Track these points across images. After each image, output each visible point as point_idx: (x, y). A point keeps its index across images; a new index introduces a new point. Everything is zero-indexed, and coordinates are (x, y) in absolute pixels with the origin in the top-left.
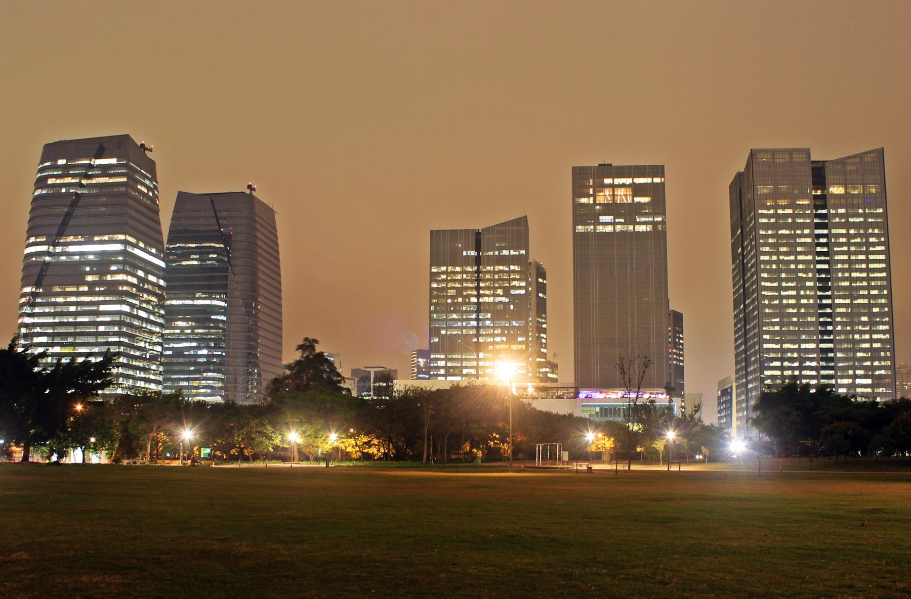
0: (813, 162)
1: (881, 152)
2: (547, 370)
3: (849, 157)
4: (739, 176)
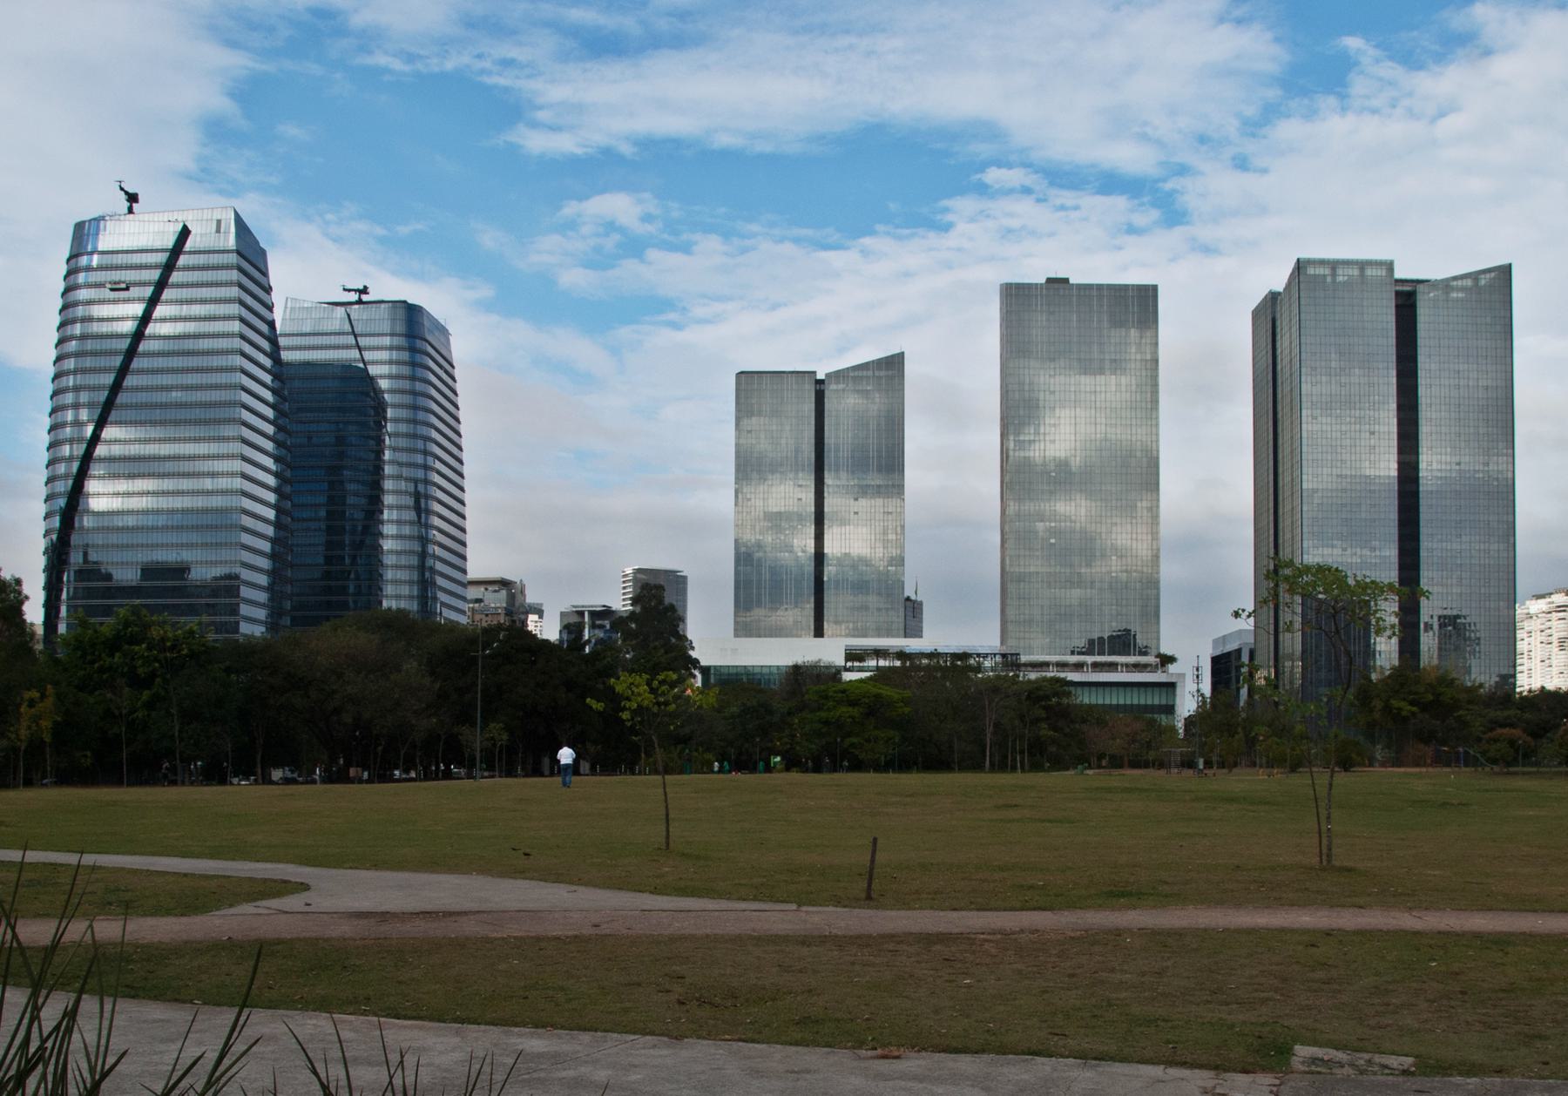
0: (1397, 281)
1: (1505, 272)
2: (848, 676)
3: (1455, 278)
4: (1273, 297)
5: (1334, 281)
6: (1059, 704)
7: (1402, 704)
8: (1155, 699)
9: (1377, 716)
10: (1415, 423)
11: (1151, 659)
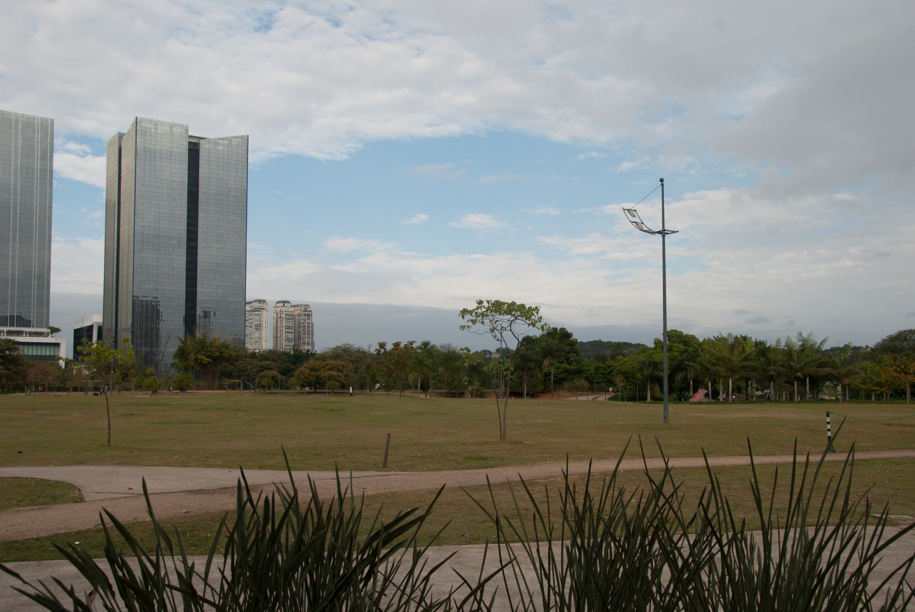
5: (156, 133)
6: (10, 355)
7: (203, 357)
8: (48, 352)
9: (192, 363)
10: (196, 210)
11: (45, 330)
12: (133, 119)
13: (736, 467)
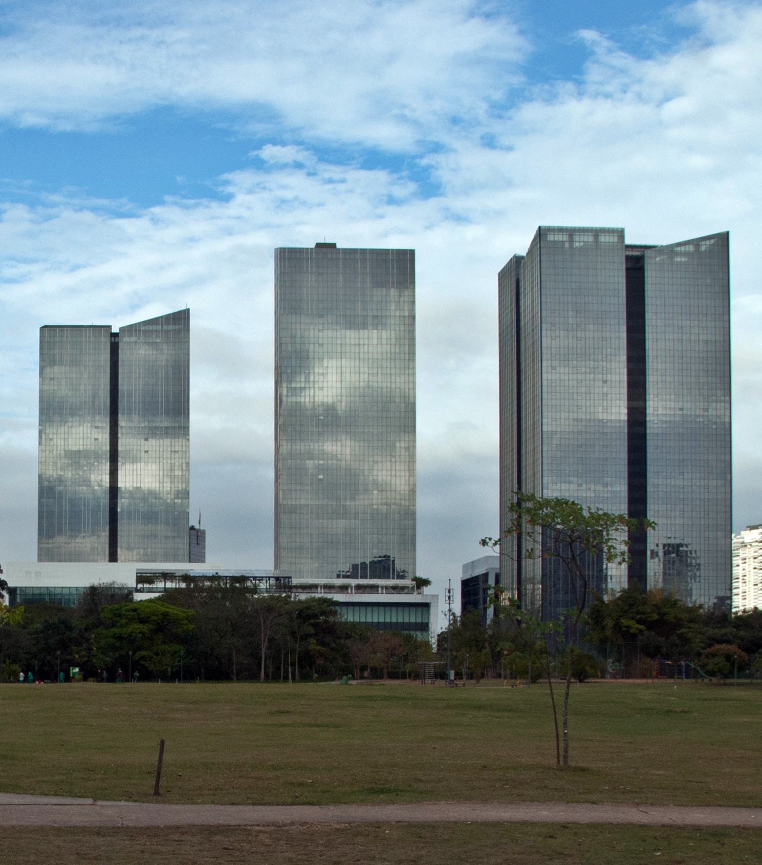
6: (326, 622)
7: (631, 623)
8: (412, 617)
9: (608, 633)
11: (408, 582)
12: (537, 228)
13: (718, 834)
